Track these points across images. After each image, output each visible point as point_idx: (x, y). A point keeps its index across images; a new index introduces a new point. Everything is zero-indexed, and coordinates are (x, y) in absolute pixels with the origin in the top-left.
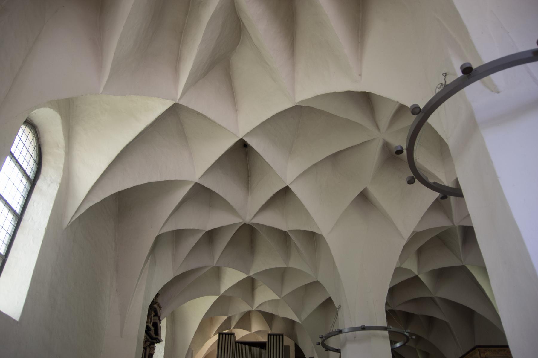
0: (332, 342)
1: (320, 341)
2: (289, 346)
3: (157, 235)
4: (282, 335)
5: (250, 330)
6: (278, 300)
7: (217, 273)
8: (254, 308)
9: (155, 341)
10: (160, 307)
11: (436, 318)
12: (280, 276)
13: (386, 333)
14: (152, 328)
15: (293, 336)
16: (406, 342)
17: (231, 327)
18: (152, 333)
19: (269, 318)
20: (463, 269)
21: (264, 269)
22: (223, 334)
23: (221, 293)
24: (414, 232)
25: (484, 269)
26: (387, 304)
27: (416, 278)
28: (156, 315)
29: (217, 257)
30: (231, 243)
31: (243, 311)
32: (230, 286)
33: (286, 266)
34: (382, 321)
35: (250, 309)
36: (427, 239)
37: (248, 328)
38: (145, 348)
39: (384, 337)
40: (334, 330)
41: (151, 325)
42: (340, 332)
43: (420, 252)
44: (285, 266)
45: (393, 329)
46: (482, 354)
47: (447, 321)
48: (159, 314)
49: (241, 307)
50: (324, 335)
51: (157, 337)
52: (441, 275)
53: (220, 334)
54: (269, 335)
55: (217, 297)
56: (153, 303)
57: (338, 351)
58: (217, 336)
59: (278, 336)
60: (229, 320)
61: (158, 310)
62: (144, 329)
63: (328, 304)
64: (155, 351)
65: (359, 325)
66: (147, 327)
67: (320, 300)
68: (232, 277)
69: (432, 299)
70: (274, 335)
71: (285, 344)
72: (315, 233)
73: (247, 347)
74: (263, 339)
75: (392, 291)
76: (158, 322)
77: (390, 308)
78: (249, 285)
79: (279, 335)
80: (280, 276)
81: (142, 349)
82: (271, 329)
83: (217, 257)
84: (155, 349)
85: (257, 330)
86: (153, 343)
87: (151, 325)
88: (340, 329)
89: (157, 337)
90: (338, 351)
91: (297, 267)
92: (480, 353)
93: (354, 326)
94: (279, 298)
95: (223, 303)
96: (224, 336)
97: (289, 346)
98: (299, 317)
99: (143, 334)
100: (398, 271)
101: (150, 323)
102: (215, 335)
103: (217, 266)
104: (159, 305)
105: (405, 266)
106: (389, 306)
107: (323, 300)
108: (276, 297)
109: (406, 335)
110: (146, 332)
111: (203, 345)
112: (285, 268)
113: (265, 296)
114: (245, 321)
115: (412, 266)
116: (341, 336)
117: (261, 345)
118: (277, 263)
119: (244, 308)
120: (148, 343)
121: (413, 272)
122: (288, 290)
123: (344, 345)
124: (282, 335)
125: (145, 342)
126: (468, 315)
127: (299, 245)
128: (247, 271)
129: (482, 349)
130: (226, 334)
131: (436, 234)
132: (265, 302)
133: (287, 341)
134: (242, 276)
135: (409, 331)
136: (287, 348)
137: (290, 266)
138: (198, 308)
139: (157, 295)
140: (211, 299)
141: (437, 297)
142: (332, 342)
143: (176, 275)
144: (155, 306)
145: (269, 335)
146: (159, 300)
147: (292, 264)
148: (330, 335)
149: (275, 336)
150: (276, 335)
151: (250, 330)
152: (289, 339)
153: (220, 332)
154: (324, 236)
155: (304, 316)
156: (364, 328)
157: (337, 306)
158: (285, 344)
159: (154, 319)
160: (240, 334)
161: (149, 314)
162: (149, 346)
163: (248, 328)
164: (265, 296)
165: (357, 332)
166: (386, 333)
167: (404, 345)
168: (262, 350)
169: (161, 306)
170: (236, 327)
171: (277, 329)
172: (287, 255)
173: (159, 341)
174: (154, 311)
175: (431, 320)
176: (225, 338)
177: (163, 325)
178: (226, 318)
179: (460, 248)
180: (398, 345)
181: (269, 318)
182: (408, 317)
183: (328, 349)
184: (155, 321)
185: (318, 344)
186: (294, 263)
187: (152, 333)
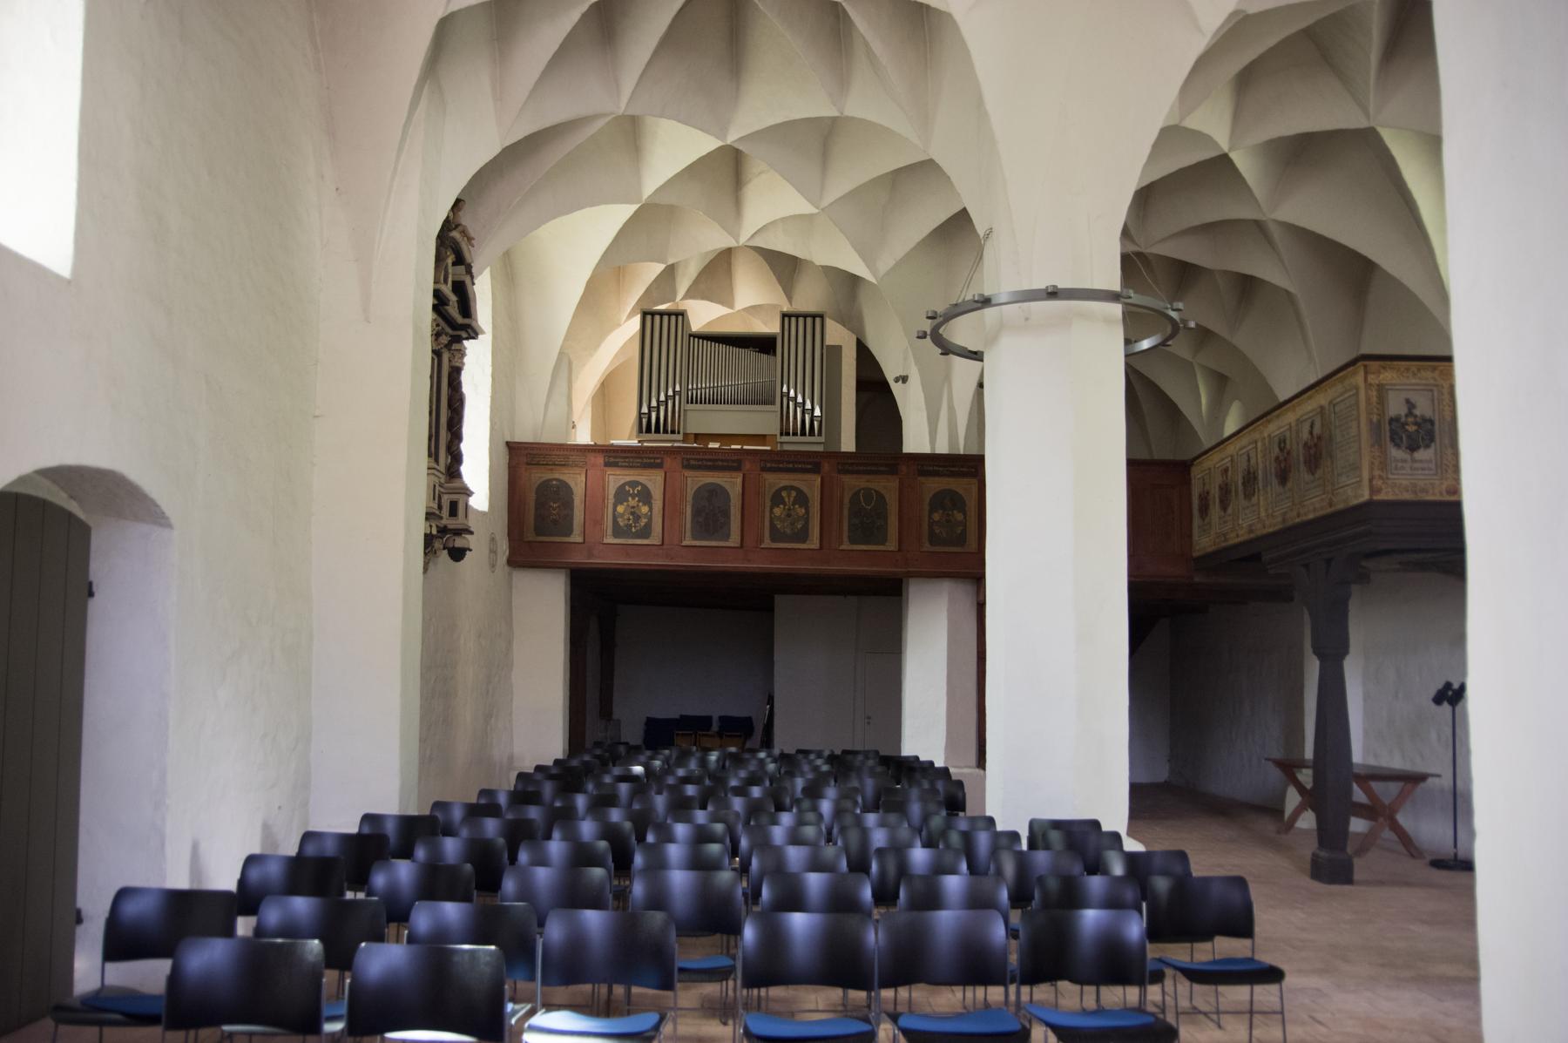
0: (962, 332)
1: (927, 326)
2: (840, 347)
3: (440, 14)
4: (822, 316)
5: (730, 304)
6: (811, 216)
7: (630, 134)
8: (743, 240)
9: (464, 335)
10: (470, 239)
11: (1263, 281)
12: (820, 140)
13: (1116, 309)
14: (453, 298)
15: (852, 320)
16: (1171, 337)
17: (674, 293)
18: (453, 310)
19: (784, 267)
20: (1367, 141)
21: (771, 122)
22: (653, 314)
23: (645, 196)
24: (1232, 15)
25: (1432, 143)
26: (1126, 233)
27: (1223, 161)
28: (460, 260)
29: (628, 82)
30: (673, 40)
31: (710, 248)
32: (670, 175)
33: (836, 114)
34: (1111, 278)
35: (729, 242)
36: (1272, 41)
37: (726, 299)
38: (437, 353)
39: (1108, 320)
40: (969, 297)
41: (447, 290)
42: (986, 302)
43: (1245, 81)
44: (831, 112)
45: (1136, 298)
46: (1372, 379)
47: (1292, 290)
48: (468, 260)
49: (703, 238)
50: (940, 309)
51: (466, 321)
52: (1299, 154)
53: (645, 314)
54: (784, 315)
55: (635, 207)
56: (448, 225)
57: (977, 356)
58: (637, 319)
59: (809, 320)
60: (670, 272)
61: (464, 246)
62: (429, 301)
63: (957, 230)
64: (466, 360)
65: (1040, 284)
66: (437, 294)
67: (936, 214)
68: (675, 147)
69: (1259, 226)
70: (797, 316)
71: (829, 341)
72: (928, 7)
73: (722, 347)
74: (771, 327)
75: (1145, 198)
76: (467, 280)
77: (1132, 248)
78: (727, 171)
79: (814, 316)
80: (820, 140)
81: (429, 354)
82: (790, 298)
83: (628, 82)
84: (463, 355)
85: (751, 304)
86: (459, 340)
87: (447, 290)
88: (987, 293)
89: (466, 321)
90: (977, 356)
91: (871, 116)
92: (1366, 373)
93: (1026, 287)
94: (815, 211)
95: (652, 220)
96: (657, 318)
97: (840, 347)
98: (870, 263)
99: (428, 315)
100: (1170, 135)
101: (446, 282)
102: (630, 316)
103: (630, 112)
104: (464, 233)
105: (1192, 123)
106: (1133, 241)
107: (943, 216)
108: (806, 208)
109: (1171, 319)
110: (435, 308)
111: (598, 346)
112: (834, 120)
113: (773, 205)
114: (717, 273)
115: (1215, 125)
116: (988, 312)
117: (764, 344)
118: (813, 104)
119: (717, 240)
120: (444, 340)
121: (1215, 144)
122: (841, 184)
123: (993, 339)
124: (822, 316)
125: (437, 335)
126: (1354, 274)
127: (877, 46)
128: (721, 133)
129: (1374, 365)
130: (662, 314)
131: (1303, 25)
132: (773, 223)
133: (836, 334)
134: (707, 144)
135: (1180, 305)
136: (836, 351)
137: (849, 112)
138: (573, 242)
139: (458, 204)
140: (621, 213)
141: (1275, 221)
142: (962, 332)
143: (507, 143)
144: (455, 234)
145: (784, 315)
146: (465, 219)
147: (855, 107)
148: (956, 311)
149: (801, 320)
150: (805, 316)
151: (730, 304)
152: (839, 327)
153: (647, 307)
154: (958, 17)
155: (886, 262)
156: (1053, 294)
157: (981, 230)
158: (829, 341)
159: (456, 272)
160: (704, 315)
161: (439, 259)
162: (448, 346)
163: (726, 299)
164: (773, 205)
165: (1033, 304)
166: (1116, 309)
167: (1163, 344)
168: (764, 357)
169: (472, 233)
170: (692, 293)
171: (808, 298)
172: (842, 82)
173: (473, 333)
174: (452, 248)
175: (1247, 286)
176: (659, 323)
177: (483, 290)
178: (660, 267)
179: (1373, 73)
180: (1145, 344)
181: (784, 267)
182: (1184, 275)
183: (947, 349)
184: (457, 279)
185: (923, 336)
186: (863, 103)
187: (453, 310)
